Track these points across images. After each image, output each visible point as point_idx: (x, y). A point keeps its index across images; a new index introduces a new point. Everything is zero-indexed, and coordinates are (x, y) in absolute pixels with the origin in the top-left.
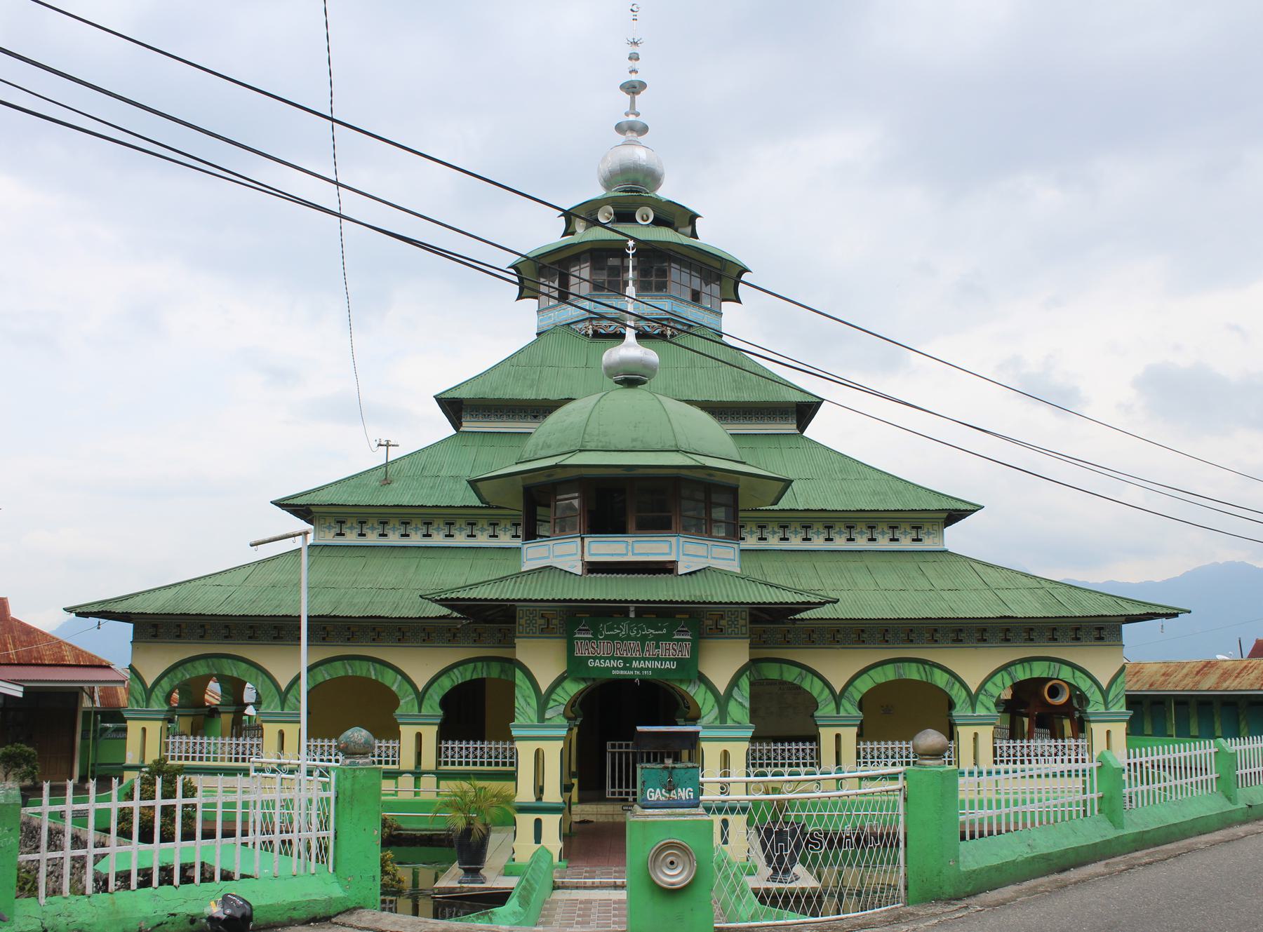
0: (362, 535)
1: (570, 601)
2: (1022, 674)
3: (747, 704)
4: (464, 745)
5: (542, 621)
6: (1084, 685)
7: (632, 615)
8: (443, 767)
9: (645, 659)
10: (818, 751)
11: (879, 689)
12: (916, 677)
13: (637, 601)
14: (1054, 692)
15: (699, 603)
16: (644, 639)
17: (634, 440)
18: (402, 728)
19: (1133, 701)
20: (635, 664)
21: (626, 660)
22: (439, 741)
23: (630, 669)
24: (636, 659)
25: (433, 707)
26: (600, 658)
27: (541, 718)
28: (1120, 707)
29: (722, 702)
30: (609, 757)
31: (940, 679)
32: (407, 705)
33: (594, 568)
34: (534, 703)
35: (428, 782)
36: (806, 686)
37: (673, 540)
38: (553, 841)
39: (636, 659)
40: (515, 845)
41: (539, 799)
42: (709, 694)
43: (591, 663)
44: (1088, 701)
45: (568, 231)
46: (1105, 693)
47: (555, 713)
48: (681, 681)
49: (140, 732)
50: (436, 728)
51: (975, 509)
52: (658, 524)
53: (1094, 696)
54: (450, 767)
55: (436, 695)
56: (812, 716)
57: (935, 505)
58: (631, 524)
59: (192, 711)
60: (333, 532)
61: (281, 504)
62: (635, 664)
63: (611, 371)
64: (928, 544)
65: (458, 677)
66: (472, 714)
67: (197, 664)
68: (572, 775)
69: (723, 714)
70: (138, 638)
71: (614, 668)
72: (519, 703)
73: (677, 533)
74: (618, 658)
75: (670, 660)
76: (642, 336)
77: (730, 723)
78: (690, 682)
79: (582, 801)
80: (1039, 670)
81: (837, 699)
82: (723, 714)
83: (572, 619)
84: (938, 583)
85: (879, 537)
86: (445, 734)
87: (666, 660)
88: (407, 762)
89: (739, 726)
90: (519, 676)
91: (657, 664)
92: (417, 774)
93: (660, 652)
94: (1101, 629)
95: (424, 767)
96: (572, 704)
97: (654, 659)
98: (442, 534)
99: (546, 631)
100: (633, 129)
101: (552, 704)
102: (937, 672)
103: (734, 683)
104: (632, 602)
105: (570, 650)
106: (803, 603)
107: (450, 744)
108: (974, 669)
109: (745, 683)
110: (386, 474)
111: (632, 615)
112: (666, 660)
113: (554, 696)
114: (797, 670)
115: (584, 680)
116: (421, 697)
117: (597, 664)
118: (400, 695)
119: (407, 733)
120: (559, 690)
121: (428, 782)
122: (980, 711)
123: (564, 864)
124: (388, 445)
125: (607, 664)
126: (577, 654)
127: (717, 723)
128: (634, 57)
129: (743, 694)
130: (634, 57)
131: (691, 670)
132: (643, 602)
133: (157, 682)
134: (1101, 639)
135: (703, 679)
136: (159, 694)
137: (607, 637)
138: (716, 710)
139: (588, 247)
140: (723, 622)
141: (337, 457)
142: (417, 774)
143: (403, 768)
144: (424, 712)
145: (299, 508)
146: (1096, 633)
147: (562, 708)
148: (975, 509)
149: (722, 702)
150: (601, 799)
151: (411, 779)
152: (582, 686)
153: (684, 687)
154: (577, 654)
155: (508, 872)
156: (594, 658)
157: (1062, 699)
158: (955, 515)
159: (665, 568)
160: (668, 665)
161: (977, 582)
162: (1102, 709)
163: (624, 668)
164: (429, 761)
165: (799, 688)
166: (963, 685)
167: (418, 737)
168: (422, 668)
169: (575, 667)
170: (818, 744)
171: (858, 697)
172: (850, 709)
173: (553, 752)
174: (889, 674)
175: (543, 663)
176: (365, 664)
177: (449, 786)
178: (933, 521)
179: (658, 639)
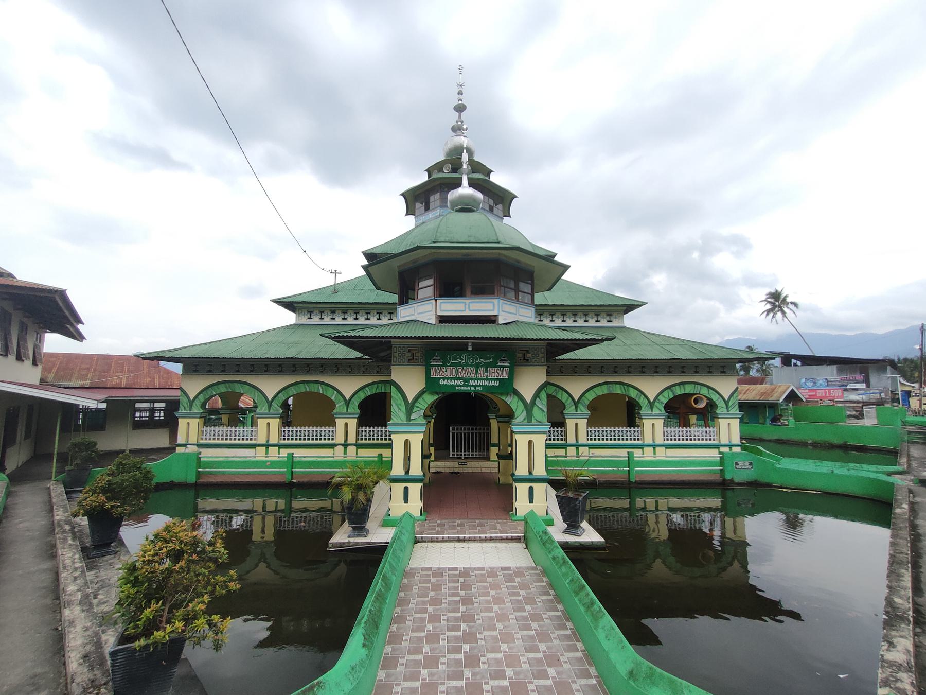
0: (321, 318)
1: (427, 338)
2: (679, 391)
3: (545, 410)
4: (372, 429)
5: (409, 355)
6: (715, 397)
7: (470, 349)
8: (360, 442)
9: (478, 379)
10: (566, 432)
11: (598, 399)
12: (619, 392)
13: (474, 338)
14: (696, 401)
15: (517, 339)
16: (477, 366)
17: (469, 236)
18: (337, 420)
19: (742, 406)
20: (471, 383)
21: (465, 380)
22: (358, 427)
23: (468, 386)
24: (472, 379)
25: (354, 409)
26: (448, 379)
27: (409, 419)
28: (735, 410)
29: (529, 408)
30: (451, 435)
31: (633, 394)
32: (340, 407)
33: (443, 320)
34: (403, 408)
35: (352, 450)
36: (559, 396)
37: (496, 301)
38: (416, 504)
39: (472, 379)
40: (391, 504)
41: (407, 472)
42: (520, 403)
43: (441, 382)
44: (717, 407)
45: (429, 176)
46: (727, 403)
47: (417, 416)
48: (502, 394)
49: (186, 425)
50: (356, 420)
51: (646, 303)
52: (483, 290)
53: (720, 403)
54: (364, 441)
55: (356, 402)
56: (562, 413)
57: (621, 303)
58: (468, 292)
59: (228, 412)
60: (306, 317)
61: (279, 302)
62: (471, 383)
63: (454, 204)
64: (615, 323)
65: (368, 392)
66: (374, 412)
67: (220, 386)
68: (430, 445)
69: (529, 416)
70: (186, 371)
71: (457, 385)
72: (394, 408)
73: (498, 297)
74: (460, 379)
75: (495, 380)
76: (471, 185)
77: (534, 422)
78: (507, 394)
79: (436, 459)
80: (689, 389)
81: (576, 404)
82: (529, 416)
83: (430, 351)
84: (627, 342)
85: (590, 320)
86: (361, 423)
87: (492, 380)
88: (340, 438)
89: (540, 423)
90: (394, 392)
91: (486, 383)
92: (345, 445)
93: (489, 375)
94: (720, 365)
95: (349, 442)
96: (431, 406)
97: (484, 379)
98: (364, 318)
99: (412, 361)
100: (457, 129)
101: (415, 409)
102: (631, 389)
103: (537, 395)
104: (470, 338)
105: (428, 373)
106: (587, 340)
107: (364, 429)
108: (652, 388)
109: (543, 395)
110: (335, 289)
111: (470, 349)
112: (492, 380)
113: (417, 404)
114: (554, 388)
115: (437, 393)
116: (347, 403)
117: (446, 382)
118: (336, 402)
119: (340, 423)
120: (420, 400)
121: (352, 450)
122: (656, 411)
123: (423, 517)
124: (336, 273)
125: (453, 382)
126: (433, 375)
127: (526, 422)
128: (460, 93)
129: (542, 404)
130: (460, 93)
131: (507, 386)
132: (478, 338)
133: (416, 399)
134: (723, 372)
135: (516, 393)
136: (198, 403)
137: (453, 365)
138: (525, 413)
139: (438, 183)
140: (529, 355)
141: (309, 280)
142: (345, 445)
143: (337, 443)
144: (349, 411)
145: (289, 304)
146: (721, 369)
147: (422, 412)
148: (646, 303)
149: (529, 408)
150: (446, 458)
151: (342, 448)
152: (436, 397)
153: (503, 398)
154: (433, 375)
155: (386, 524)
156: (444, 379)
157: (702, 405)
158: (630, 307)
159: (490, 320)
160: (493, 383)
161: (649, 342)
162: (725, 411)
163: (464, 385)
164: (352, 438)
165: (555, 397)
166: (646, 397)
167: (346, 425)
168: (348, 386)
169: (431, 384)
170: (565, 428)
171: (587, 402)
172: (583, 409)
173: (416, 441)
174: (604, 390)
175: (409, 382)
176: (316, 385)
177: (363, 452)
178: (618, 312)
179: (487, 366)
